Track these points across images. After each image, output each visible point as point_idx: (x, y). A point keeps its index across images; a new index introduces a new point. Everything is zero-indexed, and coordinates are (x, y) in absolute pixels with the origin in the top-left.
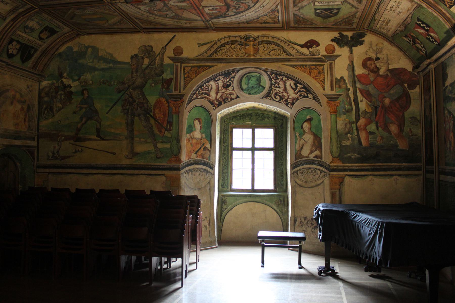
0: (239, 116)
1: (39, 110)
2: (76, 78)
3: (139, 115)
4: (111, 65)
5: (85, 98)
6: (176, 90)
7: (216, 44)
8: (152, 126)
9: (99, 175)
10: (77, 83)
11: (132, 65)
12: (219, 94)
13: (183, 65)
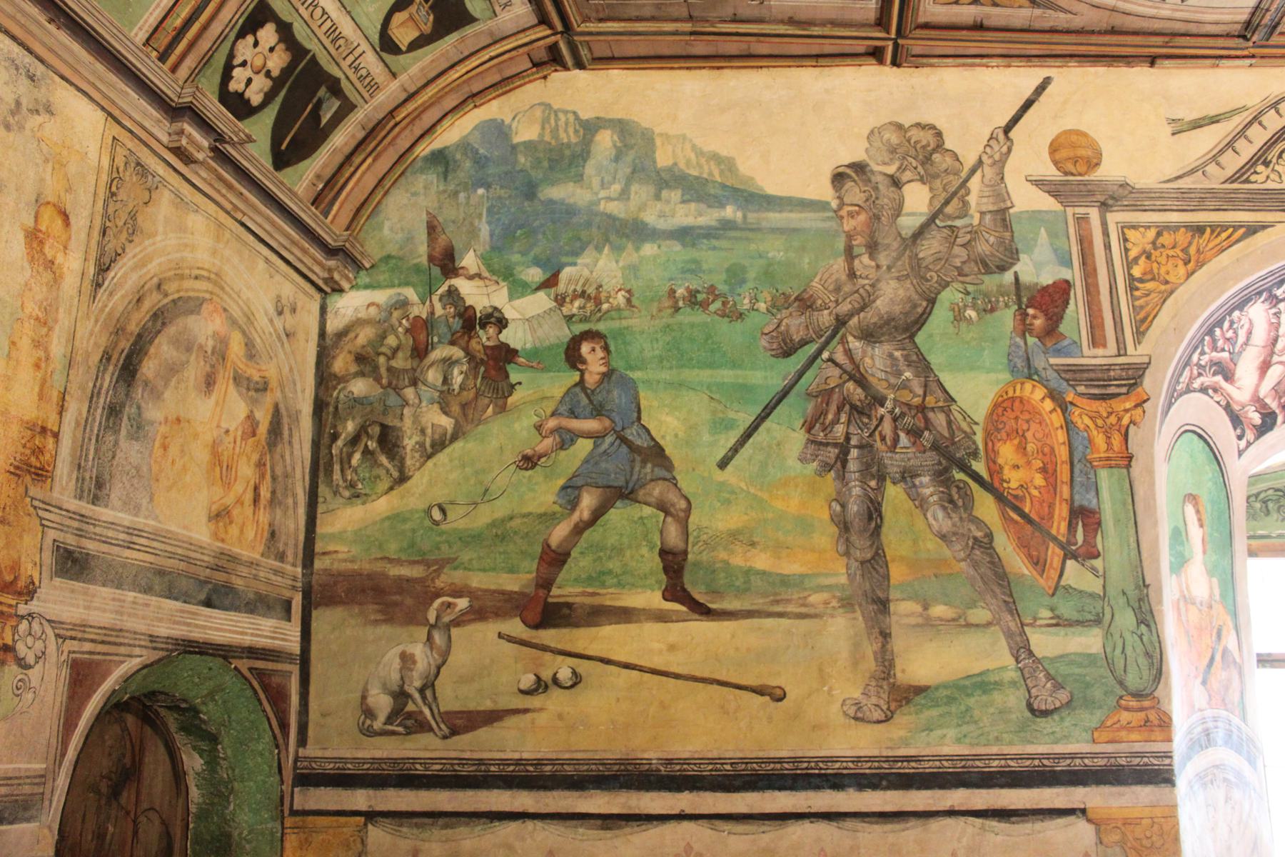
0: (1262, 496)
1: (316, 445)
2: (535, 274)
3: (907, 476)
4: (730, 212)
5: (591, 380)
6: (1097, 340)
7: (1260, 123)
8: (990, 536)
9: (686, 825)
10: (542, 301)
11: (843, 213)
12: (1270, 372)
13: (1114, 218)
